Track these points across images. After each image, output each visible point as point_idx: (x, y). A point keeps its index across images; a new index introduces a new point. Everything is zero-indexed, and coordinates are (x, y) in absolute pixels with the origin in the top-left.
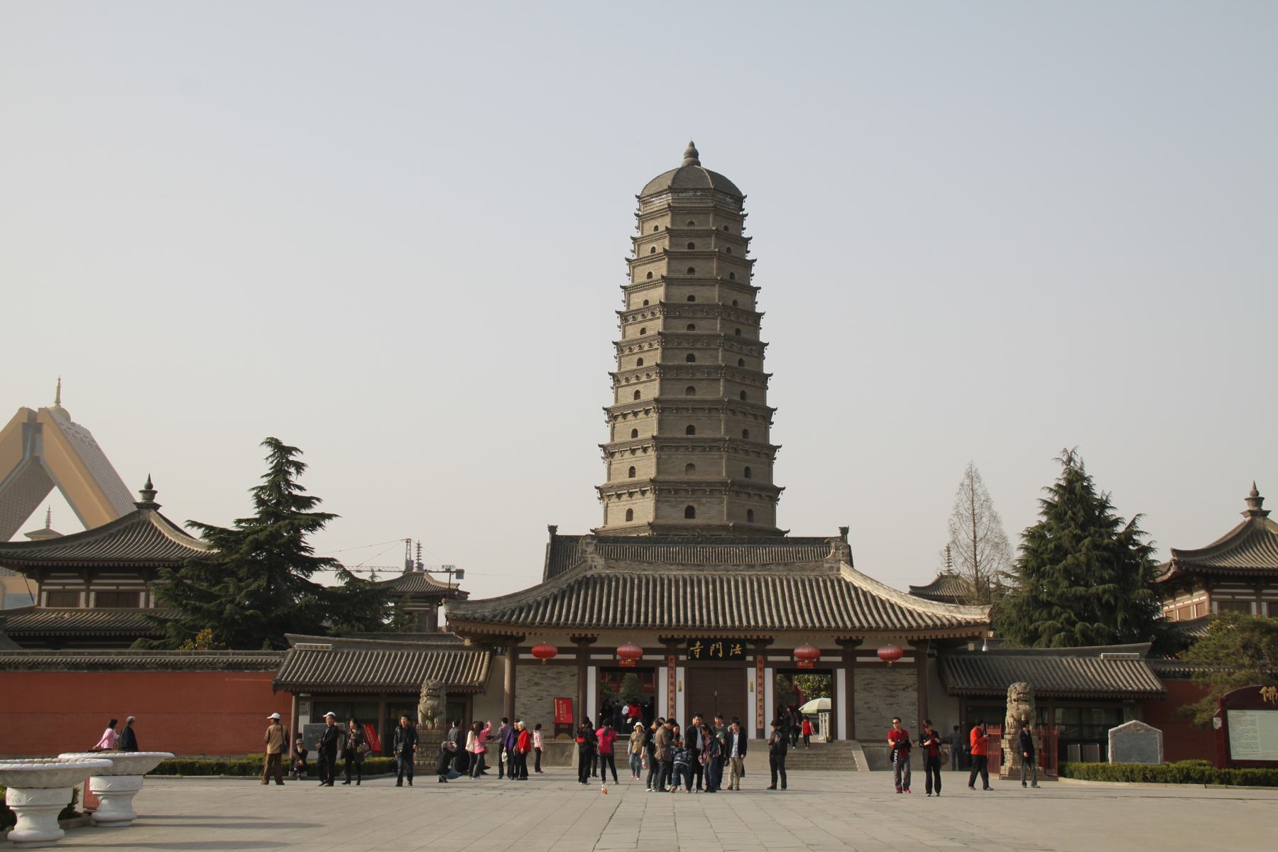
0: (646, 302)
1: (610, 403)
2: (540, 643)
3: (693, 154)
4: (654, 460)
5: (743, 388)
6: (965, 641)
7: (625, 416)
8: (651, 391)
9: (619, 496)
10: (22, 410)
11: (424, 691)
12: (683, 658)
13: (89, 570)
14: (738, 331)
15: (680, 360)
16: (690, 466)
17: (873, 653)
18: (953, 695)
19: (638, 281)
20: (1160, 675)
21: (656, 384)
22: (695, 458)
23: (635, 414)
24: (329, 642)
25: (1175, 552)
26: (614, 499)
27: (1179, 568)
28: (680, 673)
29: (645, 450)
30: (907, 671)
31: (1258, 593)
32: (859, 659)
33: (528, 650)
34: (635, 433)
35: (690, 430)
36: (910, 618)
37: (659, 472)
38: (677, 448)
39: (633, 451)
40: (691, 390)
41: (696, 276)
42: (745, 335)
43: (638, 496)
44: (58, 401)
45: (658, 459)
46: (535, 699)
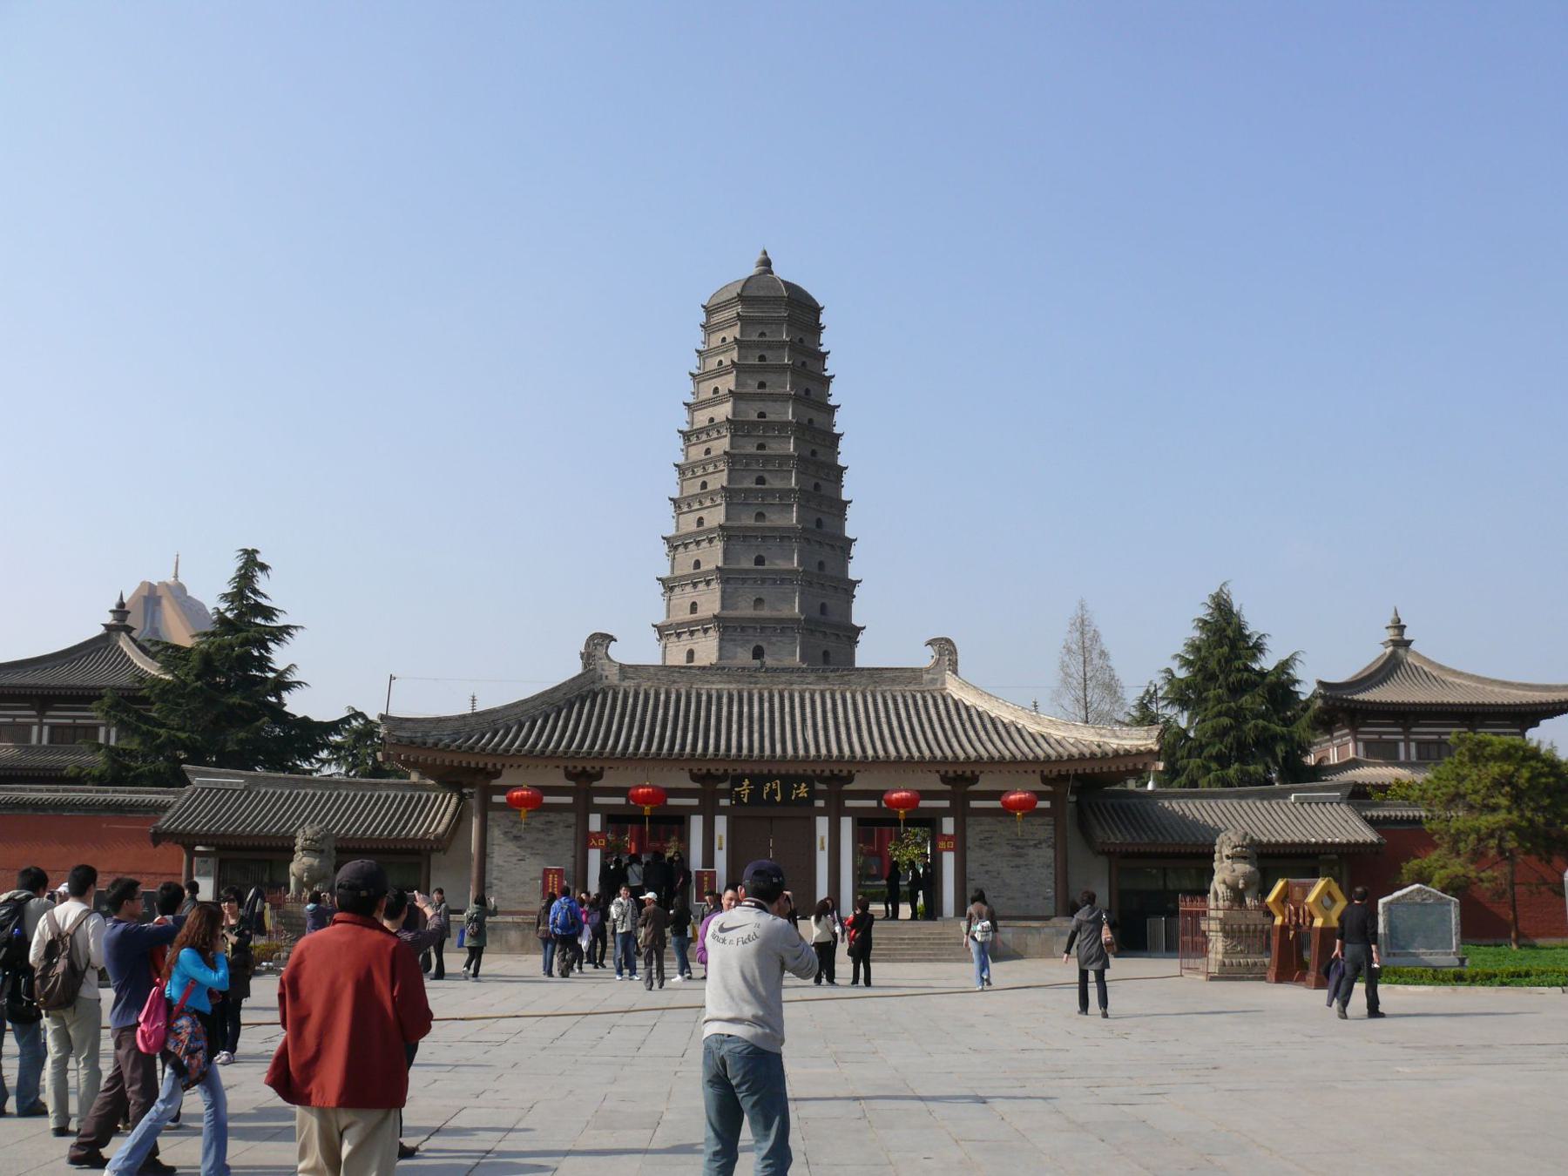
0: (712, 420)
1: (671, 532)
2: (519, 781)
3: (766, 263)
4: (719, 594)
5: (819, 515)
6: (1121, 777)
7: (686, 546)
8: (716, 516)
9: (679, 635)
10: (143, 583)
11: (300, 842)
12: (724, 802)
13: (43, 700)
14: (814, 453)
15: (748, 521)
16: (759, 602)
17: (995, 795)
18: (1103, 853)
19: (703, 397)
20: (1372, 822)
21: (722, 509)
22: (765, 592)
23: (698, 543)
24: (241, 777)
25: (1321, 684)
26: (674, 639)
27: (1326, 702)
28: (721, 824)
29: (708, 583)
30: (1040, 820)
31: (1407, 732)
32: (974, 804)
33: (504, 790)
34: (697, 564)
35: (760, 561)
36: (1045, 746)
37: (723, 607)
38: (744, 581)
39: (695, 585)
40: (760, 516)
41: (767, 391)
42: (821, 457)
43: (701, 634)
44: (176, 576)
45: (723, 592)
46: (514, 859)
